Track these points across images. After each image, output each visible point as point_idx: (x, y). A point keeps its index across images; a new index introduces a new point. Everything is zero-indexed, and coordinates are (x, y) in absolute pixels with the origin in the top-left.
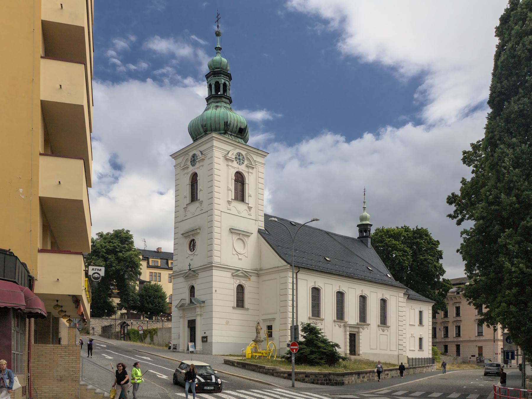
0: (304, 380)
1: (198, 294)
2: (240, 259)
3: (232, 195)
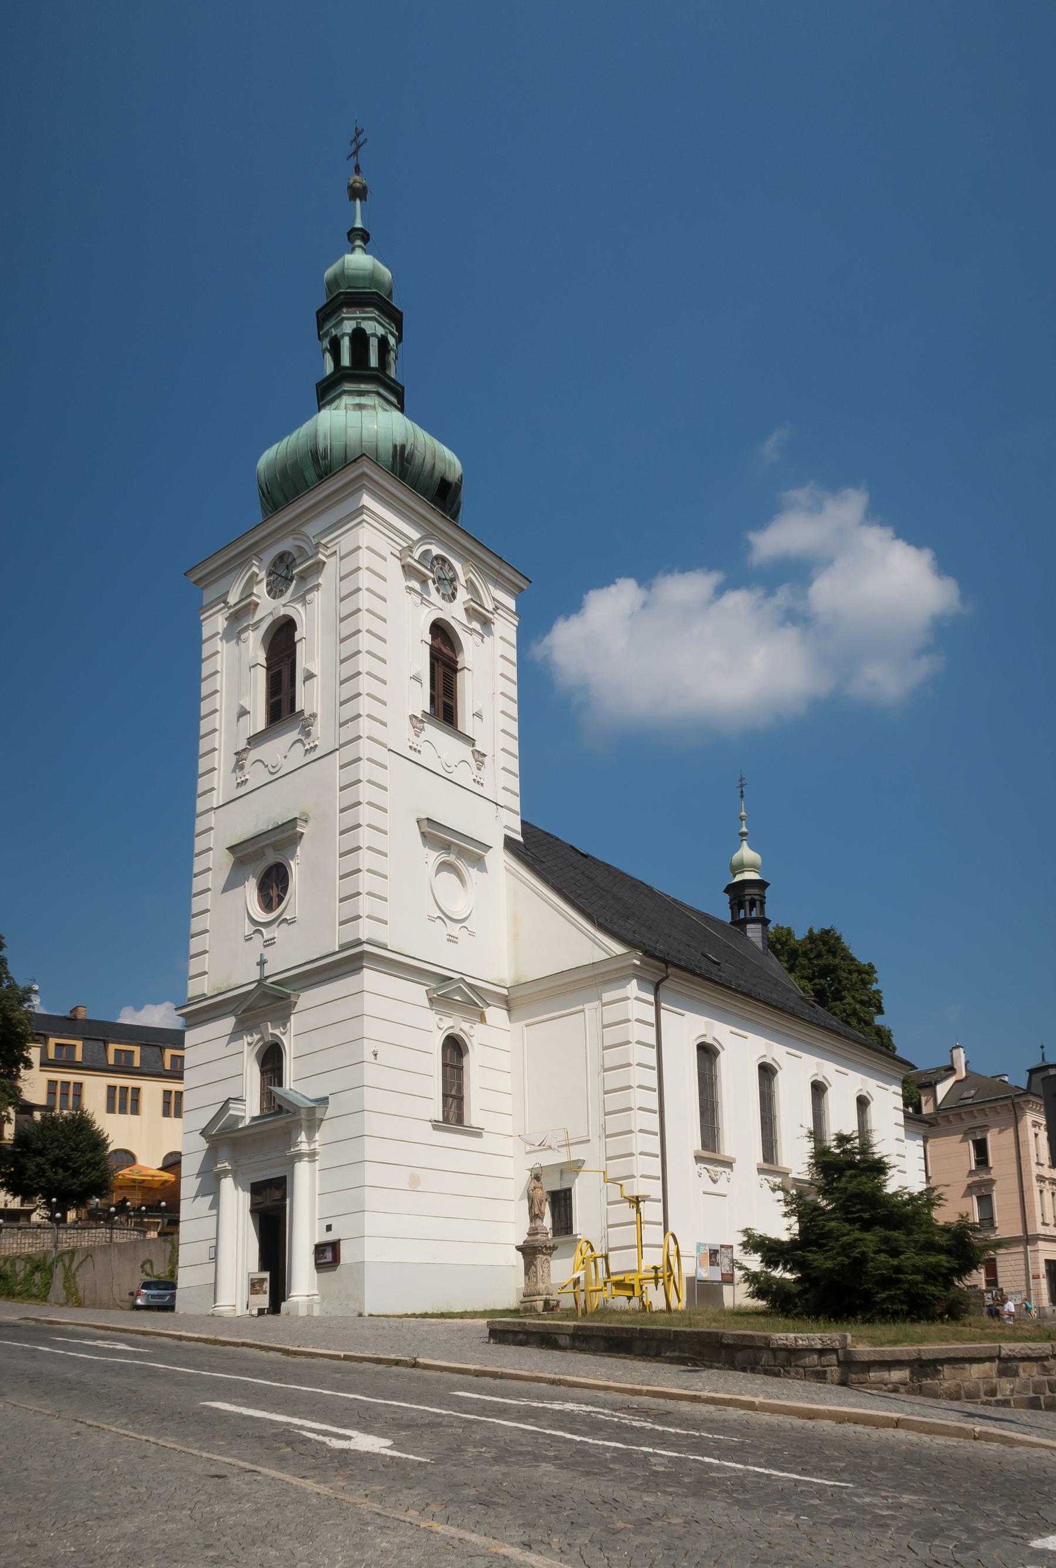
0: (992, 1392)
2: (452, 939)
3: (421, 699)
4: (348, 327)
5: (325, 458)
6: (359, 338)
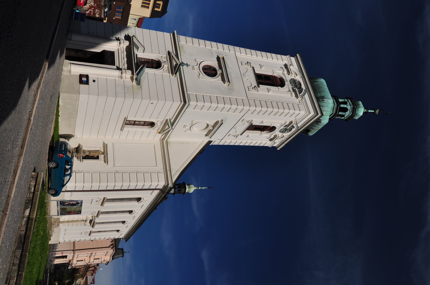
1: (148, 71)
2: (185, 126)
4: (349, 107)
5: (322, 100)
6: (345, 110)
